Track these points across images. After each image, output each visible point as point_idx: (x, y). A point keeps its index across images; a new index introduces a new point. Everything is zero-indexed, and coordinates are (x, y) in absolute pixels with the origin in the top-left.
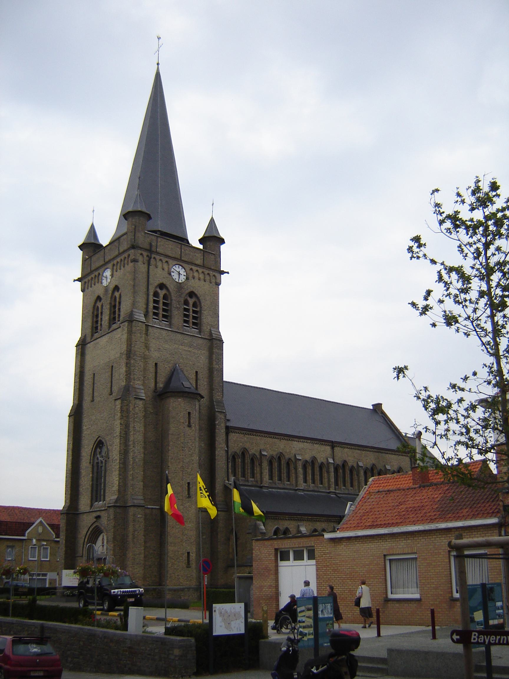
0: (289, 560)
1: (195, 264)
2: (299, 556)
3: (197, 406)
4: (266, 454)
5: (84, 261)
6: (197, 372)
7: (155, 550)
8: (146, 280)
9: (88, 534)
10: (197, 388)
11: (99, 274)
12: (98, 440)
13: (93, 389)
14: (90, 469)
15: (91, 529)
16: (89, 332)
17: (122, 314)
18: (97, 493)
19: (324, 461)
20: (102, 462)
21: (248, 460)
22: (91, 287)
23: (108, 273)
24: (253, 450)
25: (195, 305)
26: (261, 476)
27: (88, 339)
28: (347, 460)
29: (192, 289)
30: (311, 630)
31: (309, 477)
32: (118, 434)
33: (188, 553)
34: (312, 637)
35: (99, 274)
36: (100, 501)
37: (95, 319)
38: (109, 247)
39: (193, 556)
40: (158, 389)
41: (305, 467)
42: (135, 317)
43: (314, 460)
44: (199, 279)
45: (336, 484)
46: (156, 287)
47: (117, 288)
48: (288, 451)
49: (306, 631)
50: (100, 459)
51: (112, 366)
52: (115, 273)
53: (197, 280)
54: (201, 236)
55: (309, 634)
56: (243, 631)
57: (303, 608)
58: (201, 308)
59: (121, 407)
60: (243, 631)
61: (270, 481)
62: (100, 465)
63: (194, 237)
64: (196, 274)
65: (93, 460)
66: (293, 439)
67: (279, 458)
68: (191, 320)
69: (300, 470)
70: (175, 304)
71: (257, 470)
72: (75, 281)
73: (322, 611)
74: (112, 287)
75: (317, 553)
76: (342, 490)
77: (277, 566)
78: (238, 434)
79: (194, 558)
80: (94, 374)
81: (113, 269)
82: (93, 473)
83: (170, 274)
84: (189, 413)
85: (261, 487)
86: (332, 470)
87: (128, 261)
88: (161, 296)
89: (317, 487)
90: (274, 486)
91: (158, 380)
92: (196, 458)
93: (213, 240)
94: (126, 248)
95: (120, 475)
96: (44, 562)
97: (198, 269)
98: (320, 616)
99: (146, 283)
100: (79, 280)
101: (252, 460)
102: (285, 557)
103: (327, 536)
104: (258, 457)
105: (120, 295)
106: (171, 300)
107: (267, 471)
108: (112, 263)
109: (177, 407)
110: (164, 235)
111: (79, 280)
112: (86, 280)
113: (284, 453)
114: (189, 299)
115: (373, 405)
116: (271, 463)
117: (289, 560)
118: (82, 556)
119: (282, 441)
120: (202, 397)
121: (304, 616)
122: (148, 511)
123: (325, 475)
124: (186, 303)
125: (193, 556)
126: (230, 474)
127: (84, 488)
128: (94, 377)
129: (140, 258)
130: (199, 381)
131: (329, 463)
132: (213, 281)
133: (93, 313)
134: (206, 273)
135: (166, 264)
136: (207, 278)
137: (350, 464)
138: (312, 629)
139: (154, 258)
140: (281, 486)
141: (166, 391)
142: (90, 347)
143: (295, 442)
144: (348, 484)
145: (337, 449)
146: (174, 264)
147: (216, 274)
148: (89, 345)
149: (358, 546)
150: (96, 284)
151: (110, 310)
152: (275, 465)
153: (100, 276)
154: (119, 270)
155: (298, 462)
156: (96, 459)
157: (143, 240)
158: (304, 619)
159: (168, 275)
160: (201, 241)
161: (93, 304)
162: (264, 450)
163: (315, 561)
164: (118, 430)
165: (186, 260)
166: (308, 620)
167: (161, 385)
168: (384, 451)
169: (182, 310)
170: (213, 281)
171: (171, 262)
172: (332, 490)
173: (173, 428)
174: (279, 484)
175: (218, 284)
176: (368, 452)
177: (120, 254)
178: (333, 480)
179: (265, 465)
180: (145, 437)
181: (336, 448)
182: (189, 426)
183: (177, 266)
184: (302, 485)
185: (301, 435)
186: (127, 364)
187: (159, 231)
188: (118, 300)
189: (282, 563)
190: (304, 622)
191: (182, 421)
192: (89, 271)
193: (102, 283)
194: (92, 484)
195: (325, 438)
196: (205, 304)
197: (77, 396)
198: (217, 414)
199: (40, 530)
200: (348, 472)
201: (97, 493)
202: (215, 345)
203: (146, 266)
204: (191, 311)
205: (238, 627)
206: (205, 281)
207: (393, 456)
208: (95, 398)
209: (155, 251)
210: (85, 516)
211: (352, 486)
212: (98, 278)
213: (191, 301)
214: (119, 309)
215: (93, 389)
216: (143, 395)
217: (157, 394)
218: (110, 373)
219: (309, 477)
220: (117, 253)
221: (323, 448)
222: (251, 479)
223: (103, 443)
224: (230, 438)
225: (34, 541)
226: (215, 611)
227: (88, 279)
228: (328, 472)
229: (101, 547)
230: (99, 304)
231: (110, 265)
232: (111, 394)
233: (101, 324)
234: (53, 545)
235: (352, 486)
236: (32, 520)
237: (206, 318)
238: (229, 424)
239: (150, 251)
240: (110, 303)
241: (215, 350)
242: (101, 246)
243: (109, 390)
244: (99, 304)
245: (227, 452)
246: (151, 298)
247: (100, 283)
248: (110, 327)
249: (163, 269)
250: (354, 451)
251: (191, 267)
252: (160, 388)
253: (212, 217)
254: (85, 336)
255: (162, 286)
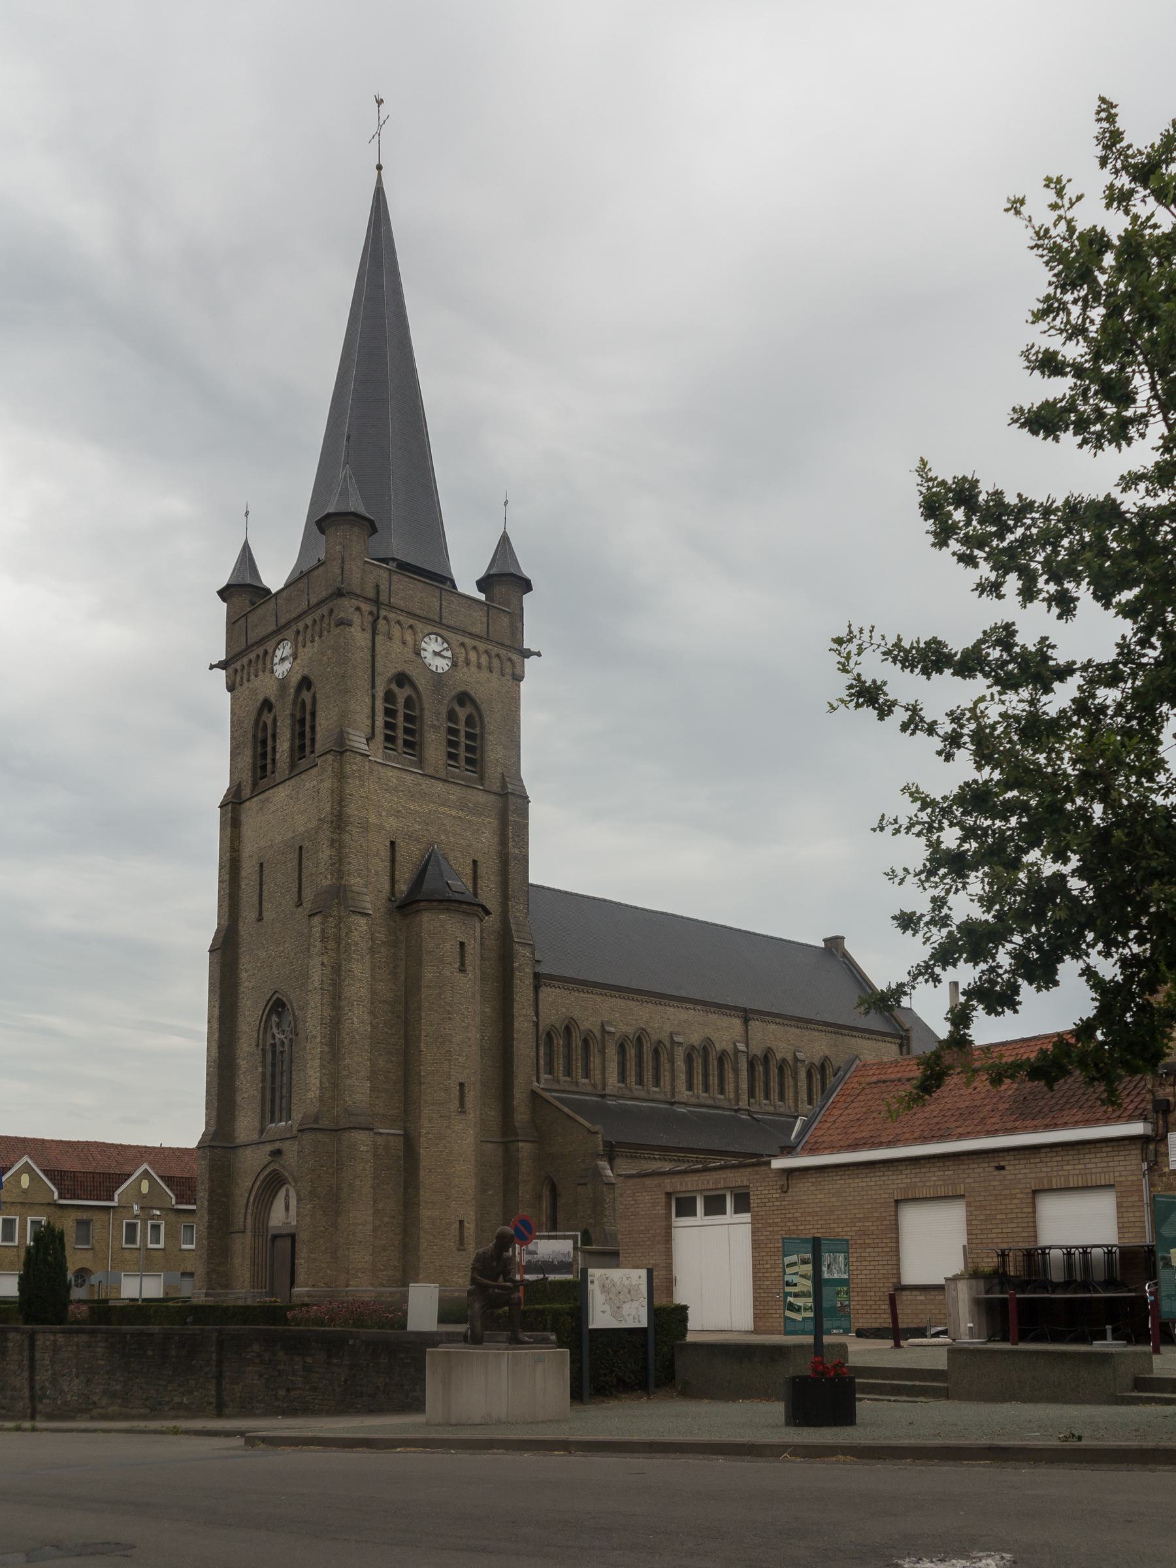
0: (695, 1215)
1: (471, 634)
2: (715, 1206)
3: (478, 930)
4: (612, 1029)
5: (232, 624)
6: (475, 862)
7: (393, 1217)
8: (369, 665)
9: (256, 1186)
10: (475, 894)
11: (266, 652)
12: (274, 998)
13: (261, 896)
14: (258, 1058)
15: (261, 1178)
16: (247, 777)
17: (319, 737)
18: (275, 1101)
19: (729, 1048)
20: (283, 1043)
21: (577, 1042)
22: (249, 680)
23: (285, 650)
24: (589, 1022)
25: (470, 721)
26: (603, 1074)
27: (247, 792)
28: (774, 1048)
29: (463, 688)
30: (809, 1302)
31: (698, 1080)
32: (317, 984)
33: (461, 1222)
34: (810, 1314)
35: (266, 652)
36: (281, 1121)
37: (259, 749)
38: (285, 594)
39: (470, 1227)
40: (398, 895)
41: (689, 1060)
42: (352, 744)
43: (706, 1048)
44: (479, 667)
45: (752, 1093)
46: (390, 681)
47: (306, 683)
48: (656, 1025)
49: (800, 1302)
50: (277, 1036)
51: (301, 848)
52: (300, 649)
53: (473, 669)
54: (481, 574)
55: (806, 1309)
56: (644, 1324)
57: (794, 1258)
58: (483, 727)
59: (323, 931)
60: (644, 1324)
61: (621, 1085)
62: (279, 1048)
63: (467, 569)
64: (473, 656)
65: (264, 1040)
66: (667, 1002)
67: (639, 1039)
68: (463, 754)
69: (681, 1065)
70: (429, 718)
71: (595, 1061)
72: (212, 667)
73: (829, 1266)
74: (295, 680)
75: (754, 1200)
76: (763, 1106)
77: (669, 1228)
78: (557, 990)
79: (472, 1231)
80: (262, 864)
81: (296, 640)
82: (264, 1066)
83: (419, 654)
84: (462, 944)
85: (603, 1096)
86: (743, 1065)
87: (329, 624)
88: (401, 701)
89: (714, 1099)
90: (627, 1093)
91: (397, 877)
92: (475, 1035)
93: (506, 582)
94: (324, 594)
95: (322, 1066)
96: (152, 1253)
97: (477, 643)
98: (826, 1275)
99: (369, 672)
100: (222, 665)
101: (586, 1042)
102: (686, 1208)
103: (777, 1164)
104: (598, 1035)
105: (314, 698)
106: (422, 710)
107: (615, 1064)
108: (294, 628)
109: (443, 932)
110: (404, 567)
111: (222, 665)
112: (238, 665)
113: (649, 1030)
114: (457, 708)
115: (824, 940)
116: (622, 1049)
117: (695, 1215)
118: (244, 1232)
119: (645, 1005)
120: (488, 913)
121: (796, 1274)
122: (379, 1140)
123: (730, 1075)
124: (452, 716)
125: (470, 1227)
126: (542, 1071)
127: (245, 1095)
128: (261, 871)
129: (356, 618)
130: (479, 881)
131: (737, 1052)
132: (508, 671)
133: (255, 736)
134: (493, 654)
135: (410, 631)
136: (496, 663)
137: (779, 1056)
138: (811, 1300)
139: (385, 618)
140: (643, 1094)
141: (419, 895)
142: (250, 810)
143: (672, 1009)
144: (774, 1095)
145: (754, 1025)
146: (426, 632)
147: (515, 657)
148: (247, 804)
149: (839, 1182)
150: (260, 673)
151: (293, 730)
152: (632, 1052)
153: (268, 658)
154: (309, 644)
155: (676, 1048)
156: (269, 1036)
157: (362, 574)
158: (796, 1279)
159: (413, 657)
160: (482, 584)
161: (253, 718)
162: (610, 1023)
163: (749, 1215)
164: (317, 975)
165: (451, 623)
166: (804, 1281)
167: (403, 888)
168: (847, 1032)
169: (443, 731)
170: (508, 671)
171: (419, 625)
172: (743, 1104)
173: (429, 974)
174: (638, 1091)
175: (518, 678)
176: (817, 1033)
177: (311, 608)
178: (744, 1086)
179: (611, 1051)
180: (373, 992)
181: (752, 1024)
182: (462, 969)
183: (433, 637)
184: (683, 1094)
185: (683, 994)
186: (333, 841)
187: (394, 559)
188: (308, 708)
189: (679, 1222)
190: (795, 1285)
191: (448, 960)
192: (244, 647)
193: (272, 672)
194: (263, 1088)
195: (729, 1001)
196: (492, 721)
197: (226, 909)
198: (517, 947)
199: (145, 1187)
200: (774, 1072)
201: (275, 1101)
202: (510, 808)
203: (368, 635)
204: (463, 734)
205: (636, 1315)
206: (491, 671)
207: (865, 1043)
208: (264, 914)
209: (386, 602)
210: (248, 1151)
211: (782, 1098)
212: (265, 661)
213: (462, 713)
214: (313, 728)
215: (261, 896)
216: (369, 908)
217: (395, 905)
218: (296, 862)
219: (698, 1080)
220: (304, 606)
221: (724, 1021)
222: (584, 1081)
223: (283, 1005)
224: (541, 996)
225: (136, 1207)
226: (592, 1282)
227: (241, 661)
228: (736, 1070)
229: (282, 1214)
230: (267, 718)
231: (290, 633)
232: (299, 904)
233: (274, 760)
234: (172, 1217)
235: (782, 1098)
236: (127, 1169)
237: (494, 753)
238: (541, 969)
239: (377, 602)
240: (292, 715)
241: (512, 817)
242: (268, 591)
243: (295, 896)
244: (267, 718)
245: (537, 1025)
246: (380, 705)
247: (267, 672)
248: (293, 765)
249: (404, 643)
250: (788, 1029)
251: (461, 638)
252: (402, 892)
253: (505, 532)
254: (239, 785)
255: (402, 679)
